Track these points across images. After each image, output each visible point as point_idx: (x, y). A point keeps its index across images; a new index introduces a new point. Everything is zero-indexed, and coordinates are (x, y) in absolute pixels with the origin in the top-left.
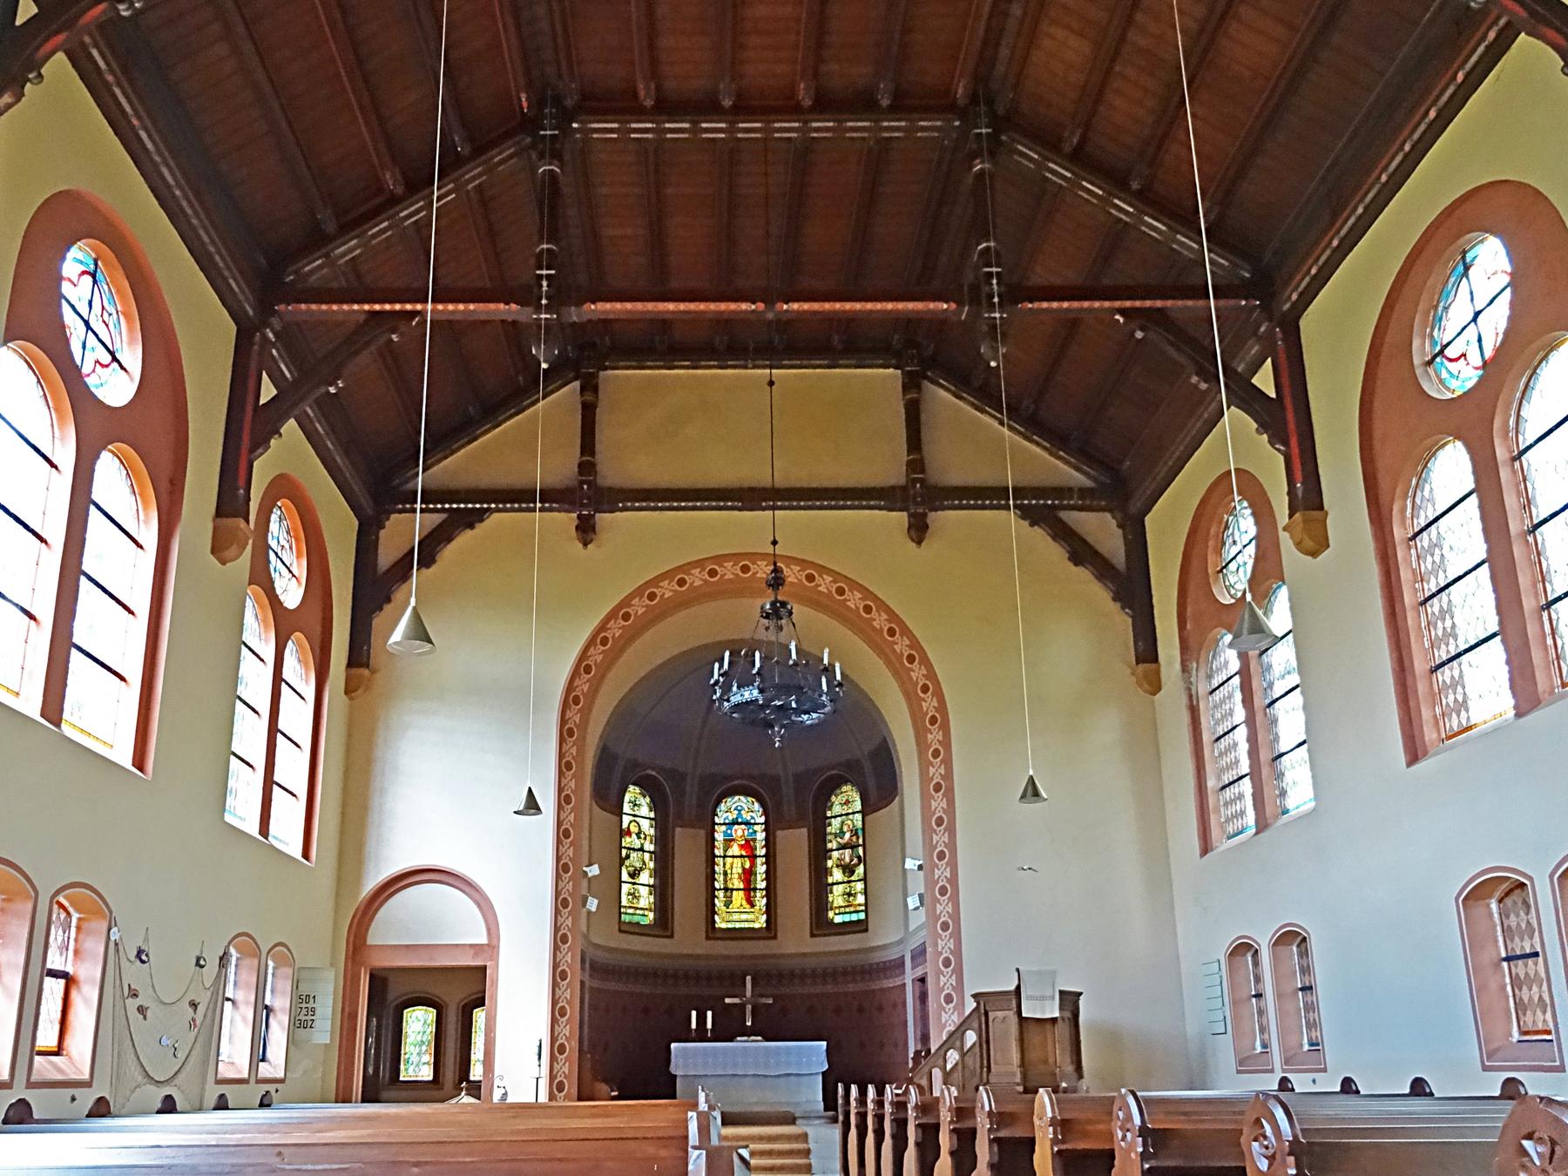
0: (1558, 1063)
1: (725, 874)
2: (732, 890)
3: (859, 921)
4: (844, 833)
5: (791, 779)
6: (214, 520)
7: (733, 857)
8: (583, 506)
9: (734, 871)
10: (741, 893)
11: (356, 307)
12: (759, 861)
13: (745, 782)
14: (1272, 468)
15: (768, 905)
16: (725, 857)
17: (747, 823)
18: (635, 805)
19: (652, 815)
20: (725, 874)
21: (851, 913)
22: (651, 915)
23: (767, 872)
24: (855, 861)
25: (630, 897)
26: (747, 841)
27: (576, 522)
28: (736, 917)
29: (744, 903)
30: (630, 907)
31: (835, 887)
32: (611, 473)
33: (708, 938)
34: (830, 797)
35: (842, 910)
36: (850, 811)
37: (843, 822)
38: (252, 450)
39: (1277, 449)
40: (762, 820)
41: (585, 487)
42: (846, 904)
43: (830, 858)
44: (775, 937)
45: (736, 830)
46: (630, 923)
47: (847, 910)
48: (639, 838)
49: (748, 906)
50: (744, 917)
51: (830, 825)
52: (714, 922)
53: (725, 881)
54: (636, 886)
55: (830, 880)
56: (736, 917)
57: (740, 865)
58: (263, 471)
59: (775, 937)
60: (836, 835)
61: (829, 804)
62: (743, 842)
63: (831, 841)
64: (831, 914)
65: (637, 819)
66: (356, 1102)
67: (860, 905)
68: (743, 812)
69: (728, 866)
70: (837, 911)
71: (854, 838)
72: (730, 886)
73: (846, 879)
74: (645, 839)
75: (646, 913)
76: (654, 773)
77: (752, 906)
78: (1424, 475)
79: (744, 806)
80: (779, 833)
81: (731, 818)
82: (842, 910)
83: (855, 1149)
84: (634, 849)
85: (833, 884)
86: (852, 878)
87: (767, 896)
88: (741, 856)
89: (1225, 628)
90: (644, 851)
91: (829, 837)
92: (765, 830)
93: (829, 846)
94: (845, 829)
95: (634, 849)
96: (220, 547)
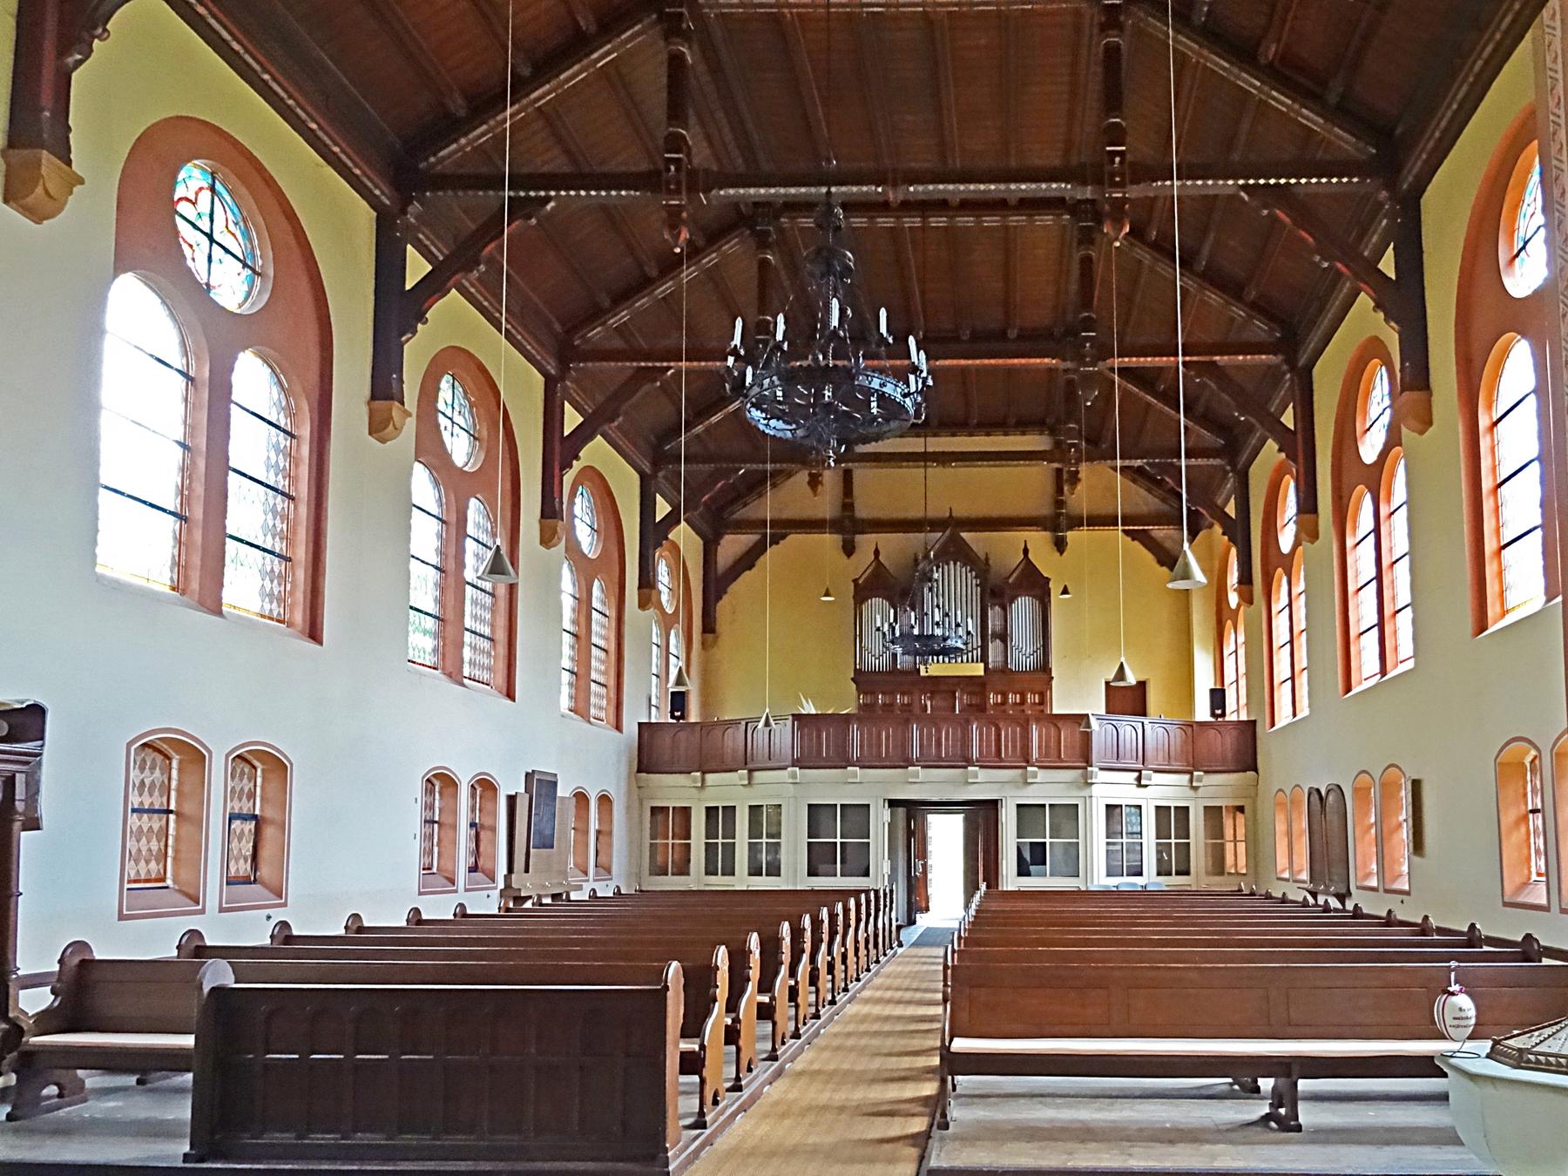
0: (125, 912)
6: (369, 403)
8: (812, 466)
11: (628, 364)
14: (1392, 338)
27: (807, 479)
32: (864, 509)
38: (562, 469)
39: (1391, 327)
41: (673, 168)
58: (416, 352)
66: (1108, 844)
83: (1330, 1150)
89: (1519, 333)
96: (379, 427)
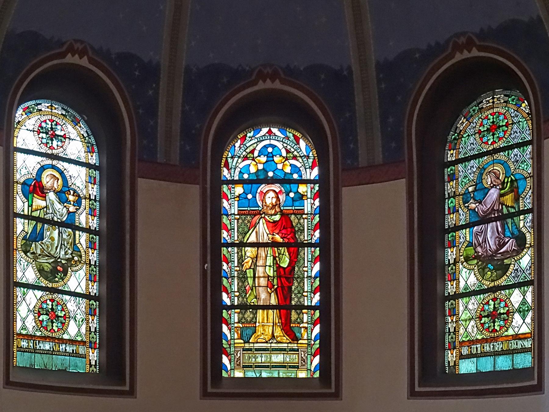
1: (243, 277)
2: (256, 308)
3: (524, 373)
4: (486, 191)
5: (373, 72)
7: (257, 245)
9: (260, 271)
10: (273, 314)
12: (307, 254)
13: (277, 85)
15: (324, 337)
16: (242, 245)
17: (285, 181)
18: (54, 136)
19: (94, 159)
20: (243, 277)
21: (496, 354)
22: (93, 356)
23: (323, 275)
24: (510, 245)
25: (44, 317)
26: (285, 215)
28: (261, 359)
29: (278, 332)
30: (45, 338)
31: (461, 302)
33: (205, 394)
34: (456, 118)
35: (477, 348)
36: (501, 144)
37: (482, 170)
40: (315, 173)
42: (487, 335)
43: (452, 245)
44: (337, 395)
45: (264, 195)
46: (31, 369)
47: (487, 348)
48: (63, 201)
49: (285, 339)
50: (278, 358)
51: (453, 177)
52: (219, 366)
53: (242, 291)
54: (58, 297)
55: (451, 288)
56: (261, 359)
57: (270, 261)
59: (337, 395)
60: (466, 197)
61: (452, 136)
62: (277, 218)
63: (455, 211)
64: (451, 356)
65: (61, 165)
67: (517, 337)
68: (277, 159)
69: (248, 262)
70: (465, 351)
71: (509, 199)
72: (252, 300)
73: (487, 284)
74: (78, 203)
75: (81, 350)
76: (84, 62)
77: (295, 338)
78: (505, 254)
79: (279, 145)
80: (345, 191)
81: (253, 170)
82: (477, 348)
84: (52, 223)
85: (458, 296)
86: (502, 282)
87: (324, 321)
88: (274, 244)
90: (76, 228)
91: (449, 203)
92: (320, 321)
93: (451, 220)
94: (488, 180)
95: (52, 223)
